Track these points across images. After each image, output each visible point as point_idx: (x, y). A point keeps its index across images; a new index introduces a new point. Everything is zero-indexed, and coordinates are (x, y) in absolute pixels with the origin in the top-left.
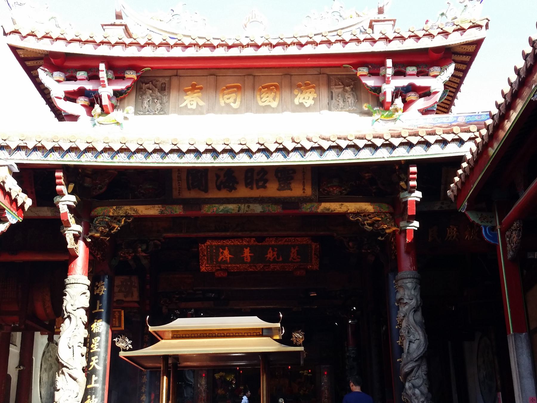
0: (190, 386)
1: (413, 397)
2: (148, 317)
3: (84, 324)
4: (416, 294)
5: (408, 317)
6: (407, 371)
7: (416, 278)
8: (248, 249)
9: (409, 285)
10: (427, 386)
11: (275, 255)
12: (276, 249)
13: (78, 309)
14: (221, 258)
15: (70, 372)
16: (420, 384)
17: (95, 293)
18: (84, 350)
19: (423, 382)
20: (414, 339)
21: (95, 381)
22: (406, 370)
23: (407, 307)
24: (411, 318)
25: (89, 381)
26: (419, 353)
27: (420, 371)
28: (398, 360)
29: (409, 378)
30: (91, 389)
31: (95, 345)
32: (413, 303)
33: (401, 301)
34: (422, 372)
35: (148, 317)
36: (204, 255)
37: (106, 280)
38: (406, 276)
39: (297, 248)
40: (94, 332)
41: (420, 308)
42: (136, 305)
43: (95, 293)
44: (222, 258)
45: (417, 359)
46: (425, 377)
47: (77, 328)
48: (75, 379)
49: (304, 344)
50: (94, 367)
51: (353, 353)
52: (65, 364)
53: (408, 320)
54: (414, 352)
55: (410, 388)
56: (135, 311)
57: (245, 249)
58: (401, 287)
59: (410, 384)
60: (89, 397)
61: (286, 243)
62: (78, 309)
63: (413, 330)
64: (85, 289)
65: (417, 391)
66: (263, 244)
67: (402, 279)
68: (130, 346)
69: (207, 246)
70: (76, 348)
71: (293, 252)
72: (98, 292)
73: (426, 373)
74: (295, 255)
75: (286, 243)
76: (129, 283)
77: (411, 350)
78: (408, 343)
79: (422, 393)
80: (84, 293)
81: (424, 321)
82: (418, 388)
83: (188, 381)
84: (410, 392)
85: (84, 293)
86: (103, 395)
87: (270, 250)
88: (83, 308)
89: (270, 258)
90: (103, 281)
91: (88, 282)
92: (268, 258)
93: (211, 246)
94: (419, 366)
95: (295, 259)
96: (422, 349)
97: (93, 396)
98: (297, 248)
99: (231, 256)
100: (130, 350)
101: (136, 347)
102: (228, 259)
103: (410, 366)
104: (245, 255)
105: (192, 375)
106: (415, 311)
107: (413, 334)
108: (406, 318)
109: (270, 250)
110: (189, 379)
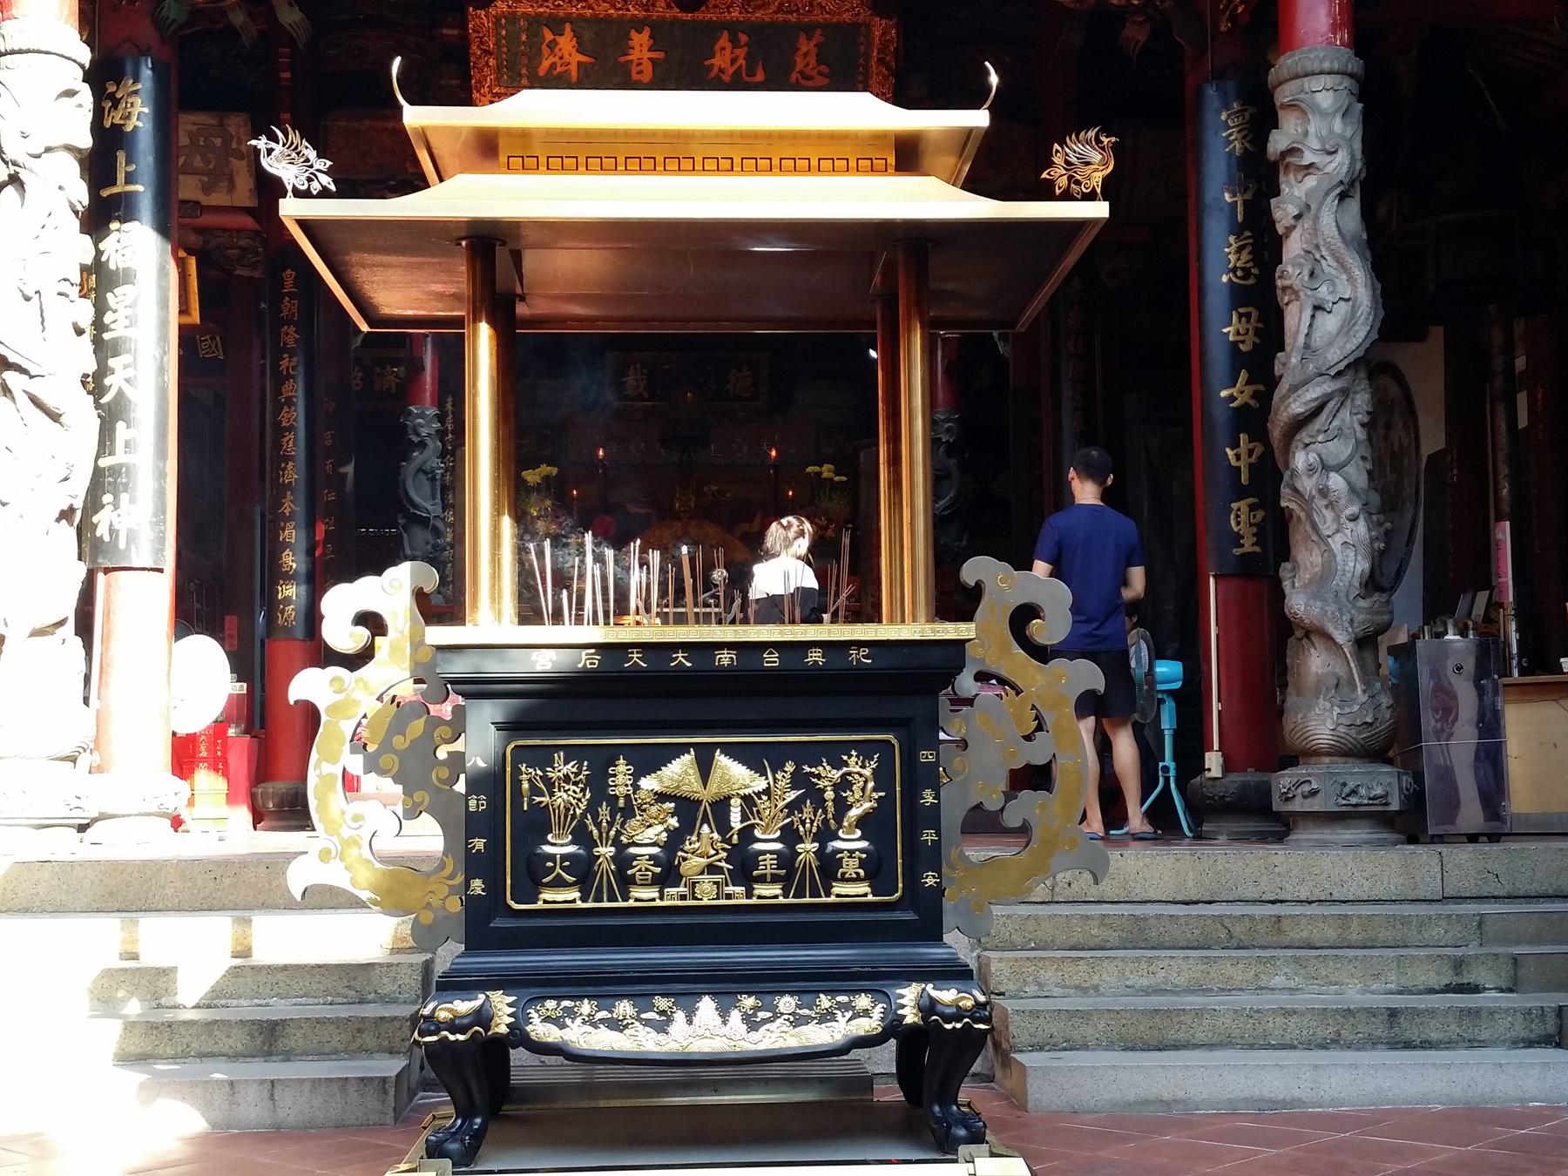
0: (424, 522)
1: (1320, 503)
2: (397, 61)
3: (76, 213)
4: (1349, 134)
5: (1316, 218)
6: (1301, 410)
7: (1351, 75)
8: (647, 32)
9: (1325, 100)
10: (1369, 466)
11: (741, 61)
12: (744, 38)
13: (48, 150)
14: (546, 64)
15: (35, 387)
16: (1343, 457)
17: (107, 124)
18: (84, 312)
19: (1356, 449)
20: (1331, 298)
21: (127, 444)
22: (1297, 407)
23: (1311, 182)
24: (1327, 220)
25: (106, 441)
26: (1350, 347)
27: (1345, 414)
28: (1224, 394)
29: (1304, 436)
30: (115, 471)
31: (120, 316)
32: (1339, 165)
33: (1290, 159)
34: (1351, 418)
35: (397, 61)
36: (487, 52)
37: (147, 73)
38: (1316, 67)
39: (818, 37)
40: (112, 266)
41: (1358, 185)
42: (248, 222)
43: (107, 124)
44: (553, 66)
45: (1341, 366)
46: (1361, 434)
47: (49, 222)
48: (55, 417)
49: (1109, 191)
50: (120, 393)
51: (948, 430)
52: (12, 358)
53: (1315, 230)
54: (1330, 344)
55: (1311, 470)
56: (243, 242)
57: (633, 33)
58: (1291, 106)
59: (1313, 457)
60: (107, 498)
61: (780, 17)
62: (48, 150)
63: (1329, 266)
64: (74, 77)
65: (1336, 481)
66: (699, 16)
67: (1297, 77)
68: (326, 180)
69: (497, 19)
70: (50, 298)
71: (804, 49)
72: (117, 121)
73: (1366, 419)
74: (813, 62)
75: (780, 17)
76: (218, 142)
77: (1318, 339)
78: (1308, 312)
79: (1352, 489)
80: (70, 93)
81: (1365, 236)
82: (1338, 468)
83: (416, 506)
84: (1307, 485)
85: (70, 93)
86: (161, 493)
87: (724, 41)
88: (69, 148)
89: (721, 71)
90: (136, 80)
91: (85, 55)
92: (716, 70)
93: (512, 18)
94: (1345, 393)
95: (812, 78)
96: (1362, 334)
97: (124, 497)
98: (818, 37)
99: (583, 58)
100: (325, 194)
101: (347, 188)
102: (574, 68)
103: (1313, 393)
104: (634, 56)
105: (427, 489)
106: (1343, 197)
107: (1331, 281)
108: (1307, 223)
109: (724, 41)
110: (418, 500)
